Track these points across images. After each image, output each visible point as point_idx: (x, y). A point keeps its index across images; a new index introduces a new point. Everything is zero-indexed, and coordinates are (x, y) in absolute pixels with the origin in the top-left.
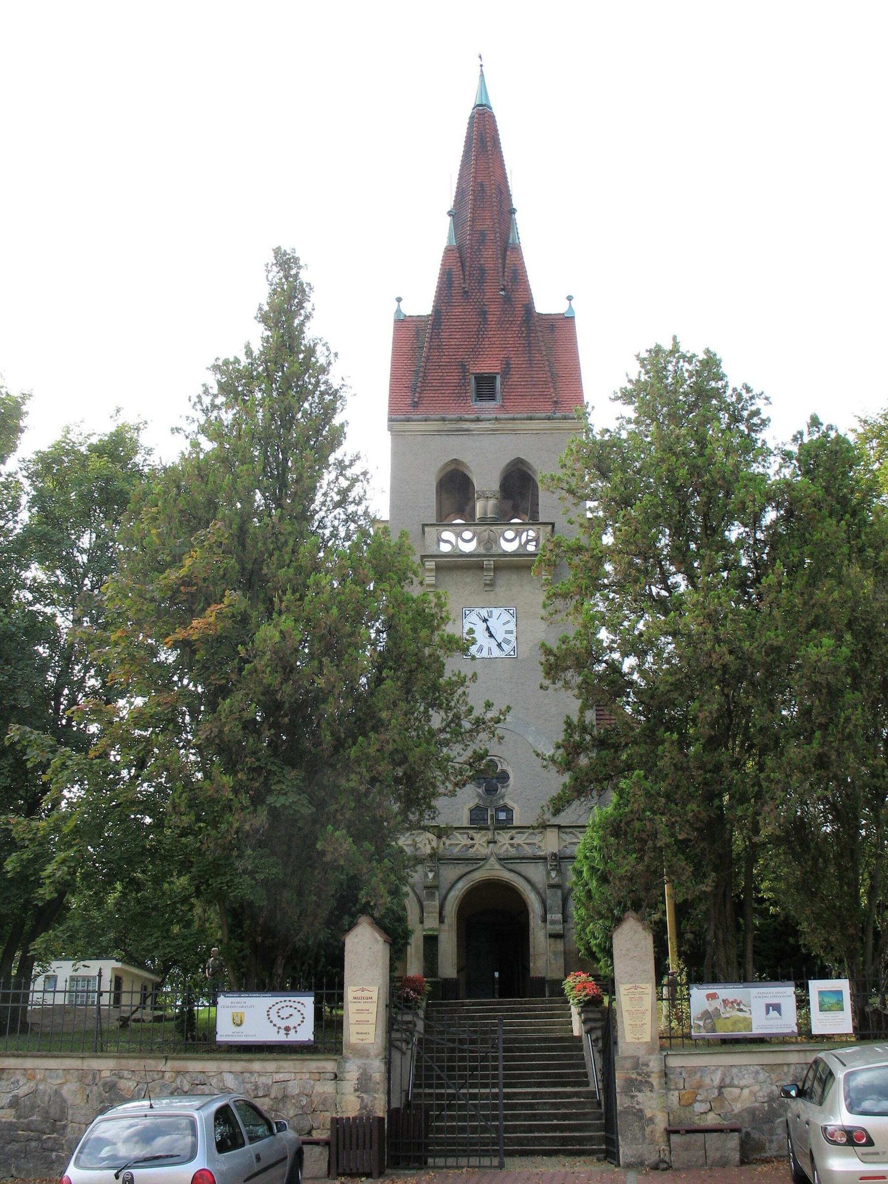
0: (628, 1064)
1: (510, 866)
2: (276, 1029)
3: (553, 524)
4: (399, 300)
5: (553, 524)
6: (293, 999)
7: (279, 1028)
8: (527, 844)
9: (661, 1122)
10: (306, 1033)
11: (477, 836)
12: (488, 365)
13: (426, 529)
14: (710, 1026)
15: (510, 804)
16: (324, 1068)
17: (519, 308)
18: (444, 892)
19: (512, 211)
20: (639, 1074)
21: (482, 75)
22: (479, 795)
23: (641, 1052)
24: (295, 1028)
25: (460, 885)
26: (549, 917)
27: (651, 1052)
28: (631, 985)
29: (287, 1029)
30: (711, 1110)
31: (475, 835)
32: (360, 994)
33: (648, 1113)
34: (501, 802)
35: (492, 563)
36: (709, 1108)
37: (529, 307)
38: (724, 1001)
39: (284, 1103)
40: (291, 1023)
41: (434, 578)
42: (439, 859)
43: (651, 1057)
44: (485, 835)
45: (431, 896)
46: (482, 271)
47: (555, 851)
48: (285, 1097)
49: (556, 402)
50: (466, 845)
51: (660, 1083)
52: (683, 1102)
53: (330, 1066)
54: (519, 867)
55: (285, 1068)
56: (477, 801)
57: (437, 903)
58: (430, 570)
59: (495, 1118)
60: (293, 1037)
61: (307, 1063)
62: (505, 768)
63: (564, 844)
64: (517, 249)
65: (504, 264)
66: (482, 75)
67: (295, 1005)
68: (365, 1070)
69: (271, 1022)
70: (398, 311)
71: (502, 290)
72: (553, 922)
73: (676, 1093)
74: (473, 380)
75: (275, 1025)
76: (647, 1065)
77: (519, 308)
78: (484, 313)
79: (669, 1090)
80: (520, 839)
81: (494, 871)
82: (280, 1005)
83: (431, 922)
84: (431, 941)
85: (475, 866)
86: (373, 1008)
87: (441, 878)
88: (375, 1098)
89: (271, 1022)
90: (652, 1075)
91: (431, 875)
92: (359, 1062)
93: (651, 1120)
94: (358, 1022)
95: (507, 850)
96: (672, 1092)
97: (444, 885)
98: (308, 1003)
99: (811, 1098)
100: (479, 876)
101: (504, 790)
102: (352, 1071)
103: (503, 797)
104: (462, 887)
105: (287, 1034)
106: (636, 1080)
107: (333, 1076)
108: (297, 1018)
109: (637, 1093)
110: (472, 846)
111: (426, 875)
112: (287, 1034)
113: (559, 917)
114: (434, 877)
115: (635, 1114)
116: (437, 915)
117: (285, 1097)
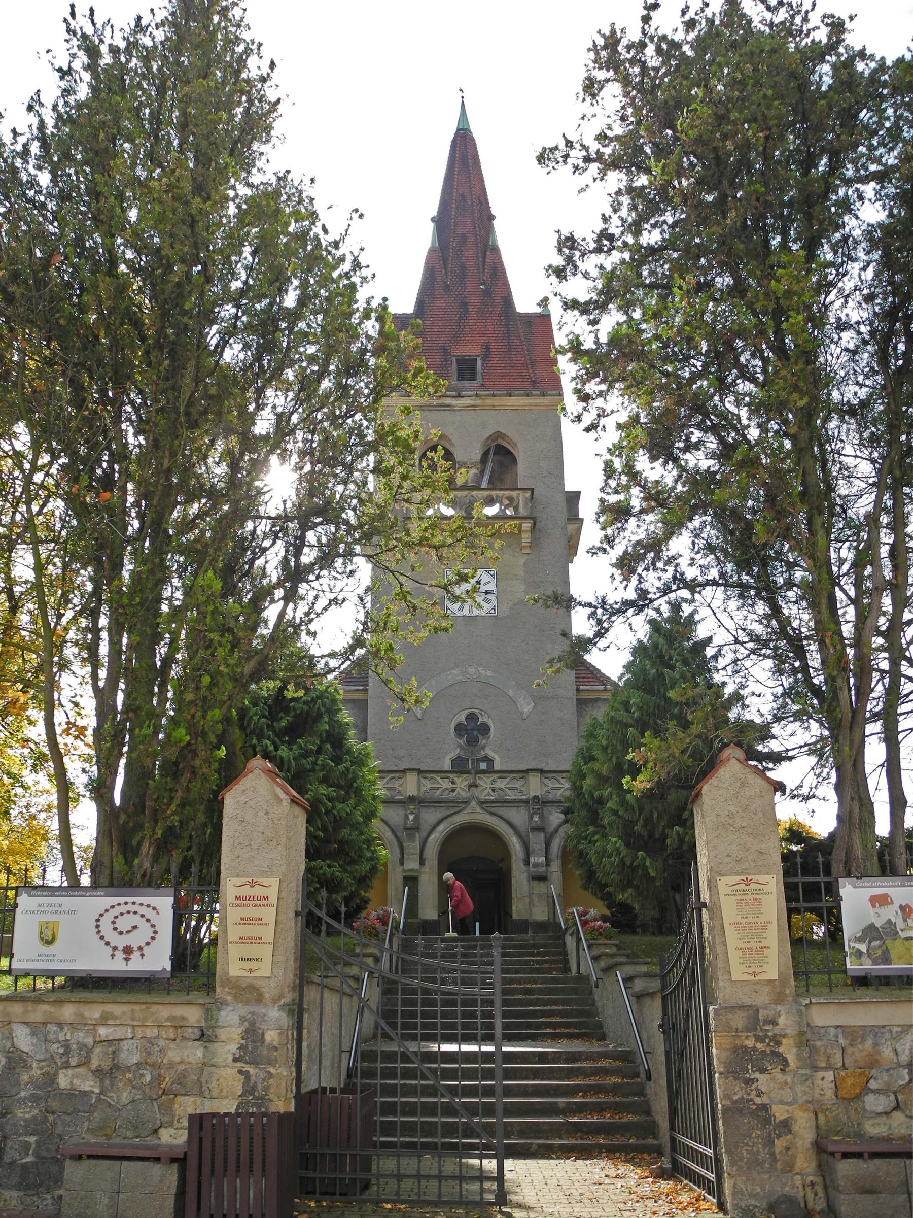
0: (739, 1020)
1: (492, 810)
2: (109, 950)
3: (532, 490)
5: (532, 490)
6: (138, 900)
7: (115, 948)
9: (805, 1131)
10: (158, 959)
11: (458, 780)
12: (470, 349)
14: (879, 952)
15: (491, 754)
16: (183, 1018)
17: (498, 299)
18: (424, 834)
19: (491, 218)
20: (758, 1039)
21: (463, 104)
22: (460, 746)
23: (762, 999)
24: (140, 948)
25: (441, 828)
26: (532, 860)
27: (779, 999)
28: (738, 878)
29: (128, 950)
30: (897, 1107)
32: (247, 891)
33: (779, 1113)
36: (893, 1104)
37: (508, 301)
38: (901, 907)
39: (113, 1079)
40: (134, 940)
42: (420, 803)
43: (779, 1008)
44: (466, 779)
45: (411, 837)
46: (463, 268)
47: (538, 794)
48: (115, 1067)
49: (534, 382)
50: (447, 789)
51: (799, 1056)
52: (843, 1093)
53: (193, 1015)
54: (502, 811)
55: (116, 1018)
56: (458, 751)
57: (417, 844)
59: (489, 1110)
60: (137, 965)
61: (154, 1008)
64: (496, 250)
65: (484, 262)
67: (136, 908)
68: (252, 1024)
69: (102, 938)
72: (536, 865)
73: (830, 1076)
75: (107, 944)
76: (774, 1022)
77: (498, 299)
78: (466, 304)
79: (815, 1068)
80: (501, 784)
81: (474, 814)
82: (117, 911)
83: (412, 864)
84: (411, 881)
85: (457, 809)
86: (269, 915)
87: (422, 821)
88: (270, 1075)
89: (102, 938)
90: (784, 1041)
91: (411, 817)
92: (243, 1010)
93: (786, 1126)
94: (243, 940)
95: (489, 795)
96: (820, 1074)
97: (425, 828)
98: (163, 904)
100: (461, 819)
102: (231, 1022)
103: (483, 748)
105: (127, 960)
106: (754, 1049)
107: (197, 1033)
108: (145, 933)
109: (757, 1075)
110: (453, 791)
111: (407, 817)
112: (127, 960)
114: (414, 819)
115: (753, 1114)
117: (115, 1067)
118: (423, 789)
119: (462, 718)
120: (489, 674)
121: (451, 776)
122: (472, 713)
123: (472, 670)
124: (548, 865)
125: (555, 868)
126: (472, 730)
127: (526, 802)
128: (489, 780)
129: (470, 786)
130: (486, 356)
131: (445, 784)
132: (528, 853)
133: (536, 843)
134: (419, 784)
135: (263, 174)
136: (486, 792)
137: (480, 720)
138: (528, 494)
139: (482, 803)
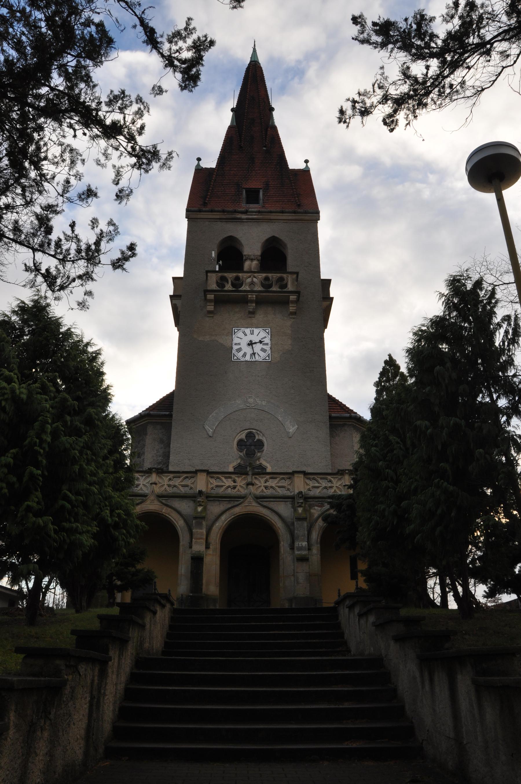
1: (265, 504)
3: (297, 273)
4: (199, 159)
8: (279, 487)
12: (253, 185)
13: (209, 274)
15: (264, 463)
22: (241, 457)
25: (223, 518)
26: (297, 544)
31: (237, 478)
34: (258, 463)
35: (254, 296)
41: (213, 307)
44: (244, 479)
45: (199, 525)
50: (229, 487)
54: (272, 505)
56: (239, 461)
57: (204, 531)
58: (210, 301)
62: (260, 438)
63: (308, 487)
66: (255, 46)
70: (198, 165)
71: (265, 147)
72: (300, 549)
74: (244, 192)
80: (272, 483)
81: (252, 507)
83: (199, 547)
84: (197, 561)
99: (110, 41)
100: (238, 510)
101: (259, 454)
103: (259, 459)
104: (225, 519)
111: (196, 509)
113: (305, 544)
116: (204, 541)
118: (210, 486)
119: (243, 436)
120: (264, 403)
121: (233, 476)
122: (251, 433)
123: (251, 400)
124: (309, 549)
125: (316, 550)
126: (251, 445)
127: (292, 498)
128: (263, 480)
129: (248, 484)
130: (266, 188)
131: (229, 482)
132: (293, 539)
133: (301, 529)
134: (207, 482)
135: (123, 422)
136: (260, 489)
137: (257, 437)
138: (295, 276)
139: (257, 498)
